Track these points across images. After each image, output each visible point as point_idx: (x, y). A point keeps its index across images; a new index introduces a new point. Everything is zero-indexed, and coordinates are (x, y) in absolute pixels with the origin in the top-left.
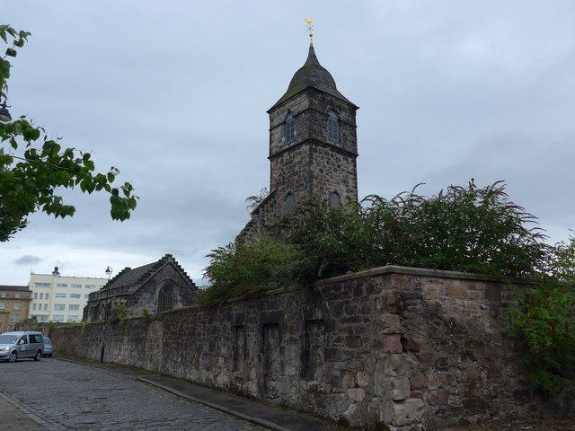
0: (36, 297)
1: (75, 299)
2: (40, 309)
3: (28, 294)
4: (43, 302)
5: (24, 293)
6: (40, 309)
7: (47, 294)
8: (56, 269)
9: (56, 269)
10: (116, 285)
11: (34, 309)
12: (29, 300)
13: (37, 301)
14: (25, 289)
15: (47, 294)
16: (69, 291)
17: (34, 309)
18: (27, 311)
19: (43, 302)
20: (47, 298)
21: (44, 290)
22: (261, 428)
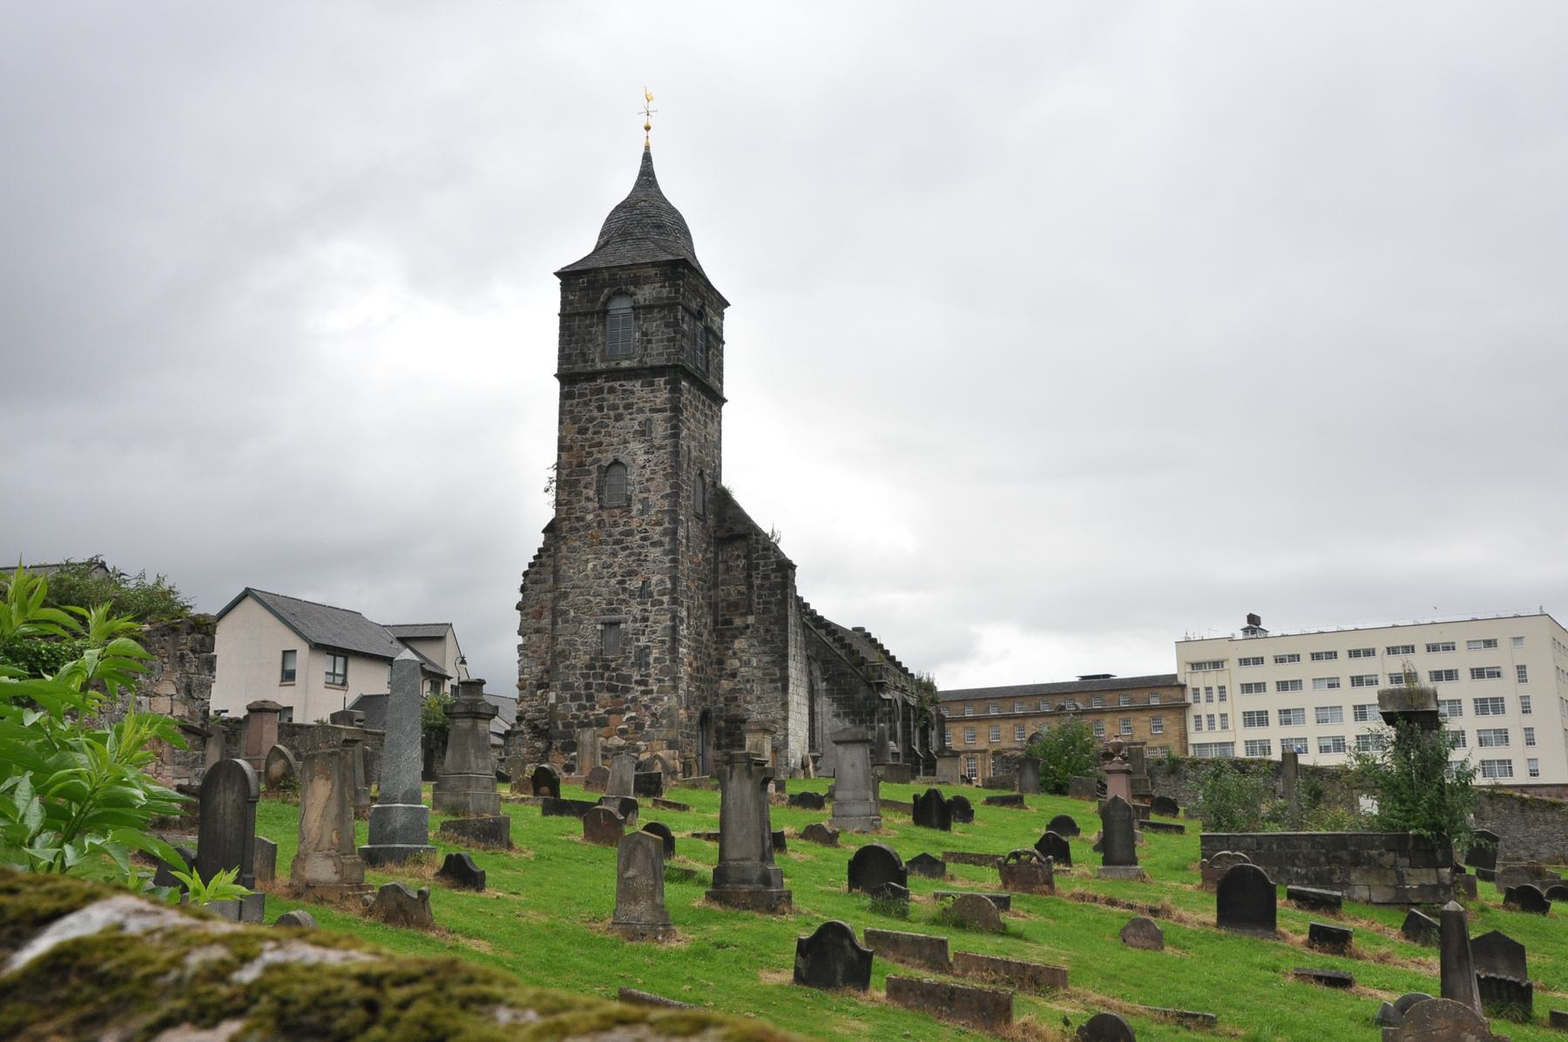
0: (1197, 699)
1: (1362, 660)
2: (1209, 699)
3: (1176, 693)
4: (1215, 708)
5: (1166, 692)
6: (1209, 699)
7: (1222, 688)
8: (1253, 620)
9: (1253, 620)
10: (277, 599)
11: (1198, 727)
12: (1183, 708)
13: (1202, 708)
14: (1166, 683)
15: (1224, 716)
16: (1345, 668)
17: (1198, 727)
18: (1184, 736)
19: (1215, 708)
20: (1223, 697)
21: (1211, 679)
22: (625, 364)
